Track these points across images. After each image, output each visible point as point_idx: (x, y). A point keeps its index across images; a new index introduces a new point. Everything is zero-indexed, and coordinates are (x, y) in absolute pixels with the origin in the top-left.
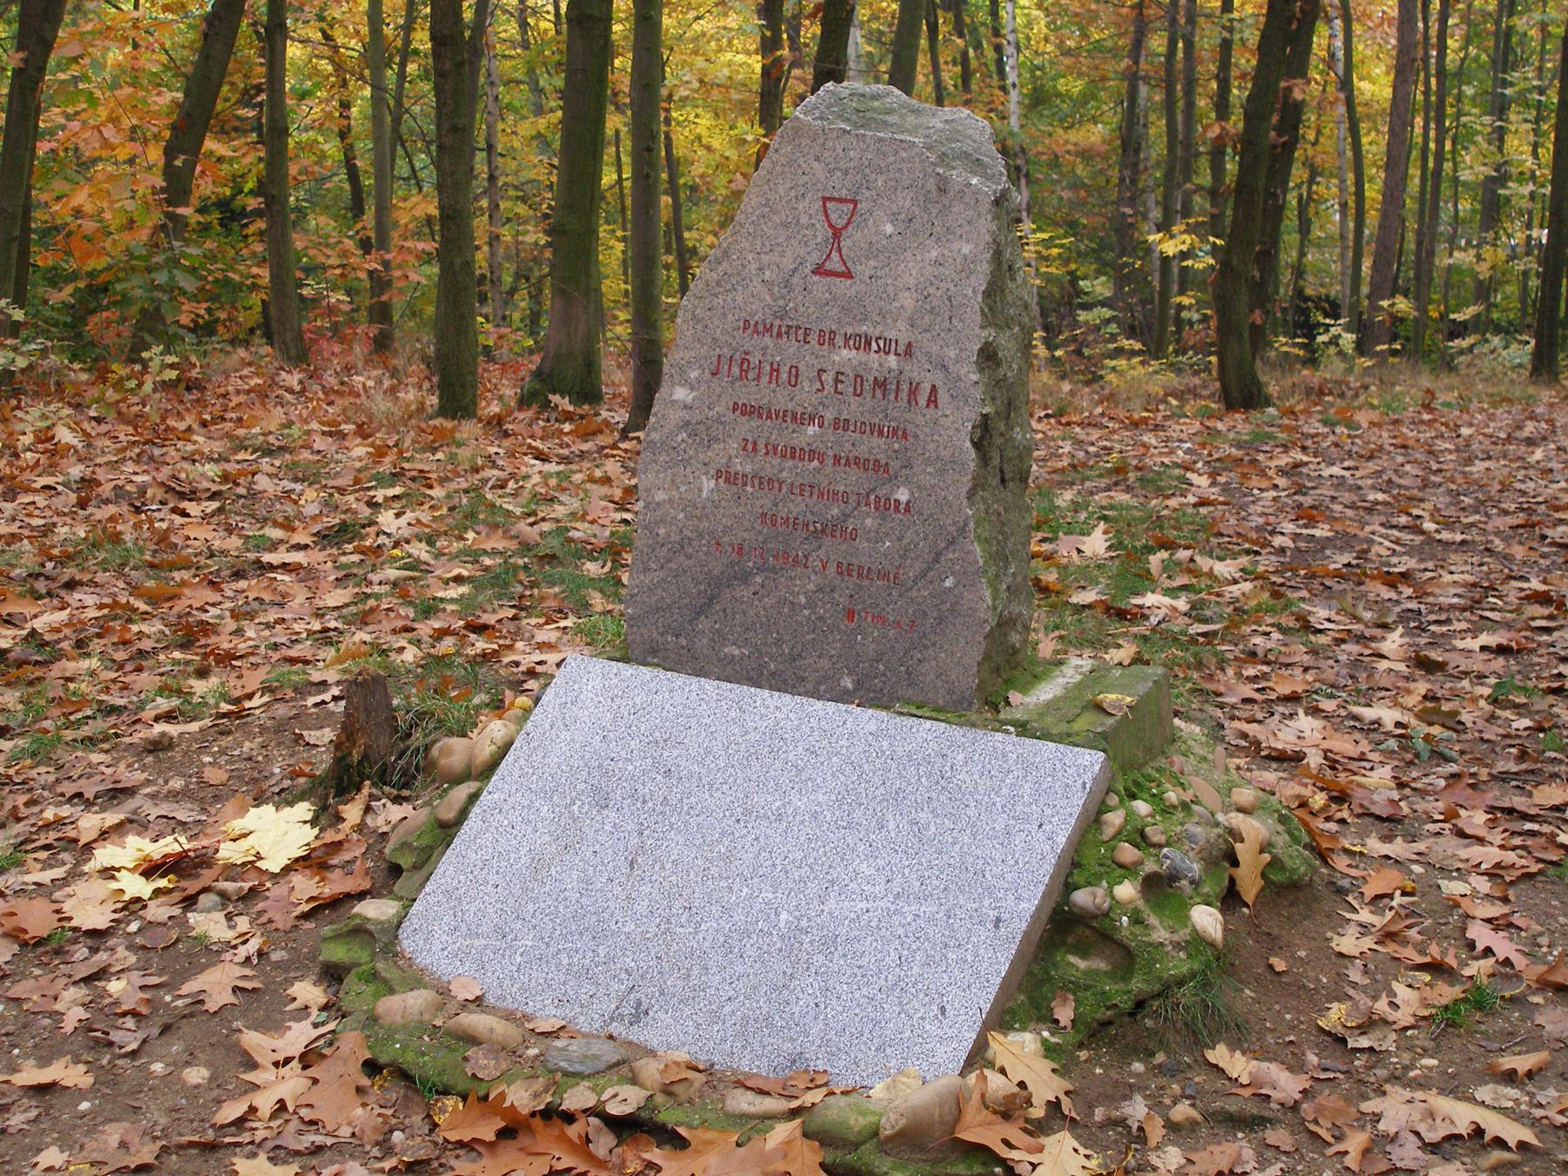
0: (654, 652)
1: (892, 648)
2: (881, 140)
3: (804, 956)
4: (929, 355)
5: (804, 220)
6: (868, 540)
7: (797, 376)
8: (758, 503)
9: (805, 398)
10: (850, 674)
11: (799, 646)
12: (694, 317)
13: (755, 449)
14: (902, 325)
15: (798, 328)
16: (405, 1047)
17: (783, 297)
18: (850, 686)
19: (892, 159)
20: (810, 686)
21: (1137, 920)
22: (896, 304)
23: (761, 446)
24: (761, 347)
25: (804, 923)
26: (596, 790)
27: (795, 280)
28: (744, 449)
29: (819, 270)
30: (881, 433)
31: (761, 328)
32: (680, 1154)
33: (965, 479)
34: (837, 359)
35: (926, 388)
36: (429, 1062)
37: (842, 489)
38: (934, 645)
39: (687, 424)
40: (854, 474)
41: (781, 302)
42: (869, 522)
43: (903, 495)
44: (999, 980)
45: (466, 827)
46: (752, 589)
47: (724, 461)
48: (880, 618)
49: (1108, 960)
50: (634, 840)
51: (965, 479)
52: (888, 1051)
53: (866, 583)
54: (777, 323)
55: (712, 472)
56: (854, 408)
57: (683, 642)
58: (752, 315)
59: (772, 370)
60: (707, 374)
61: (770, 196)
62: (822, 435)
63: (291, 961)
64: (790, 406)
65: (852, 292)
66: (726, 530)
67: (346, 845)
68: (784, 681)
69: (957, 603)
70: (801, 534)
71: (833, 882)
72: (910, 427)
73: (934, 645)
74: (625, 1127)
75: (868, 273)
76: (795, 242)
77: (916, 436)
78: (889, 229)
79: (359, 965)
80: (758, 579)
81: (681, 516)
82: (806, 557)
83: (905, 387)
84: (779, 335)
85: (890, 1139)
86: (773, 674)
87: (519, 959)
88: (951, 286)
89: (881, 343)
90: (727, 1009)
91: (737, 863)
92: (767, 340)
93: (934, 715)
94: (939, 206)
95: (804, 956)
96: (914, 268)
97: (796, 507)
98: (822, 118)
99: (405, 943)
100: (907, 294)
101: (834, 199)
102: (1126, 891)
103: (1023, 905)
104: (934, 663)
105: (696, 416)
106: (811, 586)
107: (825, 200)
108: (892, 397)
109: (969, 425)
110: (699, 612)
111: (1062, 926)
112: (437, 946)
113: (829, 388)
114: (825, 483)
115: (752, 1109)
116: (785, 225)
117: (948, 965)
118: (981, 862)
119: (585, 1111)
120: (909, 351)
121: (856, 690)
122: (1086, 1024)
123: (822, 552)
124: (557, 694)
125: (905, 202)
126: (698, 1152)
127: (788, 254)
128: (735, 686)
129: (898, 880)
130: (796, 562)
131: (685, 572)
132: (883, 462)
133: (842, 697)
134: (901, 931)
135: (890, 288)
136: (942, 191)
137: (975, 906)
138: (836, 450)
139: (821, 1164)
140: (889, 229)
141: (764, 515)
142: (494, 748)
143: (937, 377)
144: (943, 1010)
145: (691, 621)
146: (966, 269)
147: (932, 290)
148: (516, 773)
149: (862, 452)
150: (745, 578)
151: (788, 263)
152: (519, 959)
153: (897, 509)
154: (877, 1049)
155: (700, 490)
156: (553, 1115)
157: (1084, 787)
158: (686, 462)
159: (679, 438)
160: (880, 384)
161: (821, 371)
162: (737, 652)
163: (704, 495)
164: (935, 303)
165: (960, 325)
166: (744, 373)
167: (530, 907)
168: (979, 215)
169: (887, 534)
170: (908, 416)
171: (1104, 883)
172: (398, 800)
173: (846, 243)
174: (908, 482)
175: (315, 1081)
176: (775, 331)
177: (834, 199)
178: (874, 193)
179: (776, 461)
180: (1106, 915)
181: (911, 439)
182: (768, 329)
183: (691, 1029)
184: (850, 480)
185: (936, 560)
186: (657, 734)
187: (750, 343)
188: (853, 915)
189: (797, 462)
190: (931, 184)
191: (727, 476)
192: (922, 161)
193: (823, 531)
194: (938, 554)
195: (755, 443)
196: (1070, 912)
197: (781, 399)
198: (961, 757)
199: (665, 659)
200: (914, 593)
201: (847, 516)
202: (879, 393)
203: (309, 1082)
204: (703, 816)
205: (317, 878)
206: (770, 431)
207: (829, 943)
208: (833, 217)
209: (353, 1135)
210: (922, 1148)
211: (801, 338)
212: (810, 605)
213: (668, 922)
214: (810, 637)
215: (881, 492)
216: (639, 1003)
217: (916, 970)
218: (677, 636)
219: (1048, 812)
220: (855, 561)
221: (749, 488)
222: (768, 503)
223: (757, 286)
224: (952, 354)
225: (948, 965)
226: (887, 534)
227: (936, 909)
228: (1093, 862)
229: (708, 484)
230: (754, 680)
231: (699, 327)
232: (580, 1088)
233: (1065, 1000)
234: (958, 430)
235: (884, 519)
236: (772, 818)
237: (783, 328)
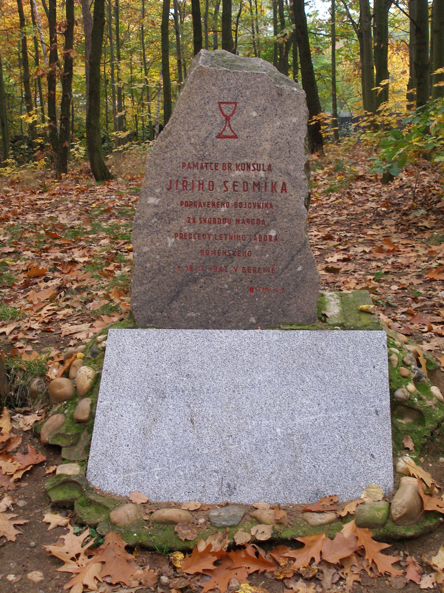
0: (150, 321)
1: (274, 302)
2: (246, 74)
3: (297, 446)
4: (280, 169)
5: (210, 113)
6: (257, 255)
7: (213, 186)
8: (198, 246)
9: (219, 194)
10: (253, 316)
11: (227, 308)
12: (155, 164)
13: (194, 221)
14: (266, 157)
15: (212, 163)
16: (139, 535)
17: (202, 150)
18: (254, 321)
19: (253, 82)
20: (234, 325)
21: (420, 399)
22: (261, 148)
23: (197, 220)
24: (191, 175)
25: (289, 431)
26: (156, 391)
27: (208, 142)
28: (189, 222)
29: (220, 136)
30: (259, 207)
31: (192, 166)
32: (301, 550)
33: (303, 222)
34: (233, 175)
35: (280, 184)
36: (157, 539)
37: (241, 234)
38: (295, 297)
39: (156, 214)
40: (247, 227)
41: (201, 153)
42: (257, 247)
43: (273, 233)
44: (390, 437)
45: (97, 421)
46: (199, 285)
47: (178, 229)
48: (267, 289)
49: (411, 417)
50: (188, 410)
51: (303, 222)
52: (357, 479)
53: (258, 274)
54: (200, 162)
55: (172, 235)
56: (244, 197)
57: (165, 314)
58: (187, 159)
59: (200, 184)
60: (165, 190)
61: (191, 104)
62: (228, 211)
63: (30, 505)
64: (211, 200)
65: (238, 144)
66: (183, 260)
67: (12, 441)
68: (220, 324)
69: (304, 277)
70: (222, 257)
71: (293, 410)
72: (273, 202)
73: (295, 297)
74: (272, 544)
75: (245, 135)
76: (206, 124)
77: (277, 206)
78: (254, 114)
79: (77, 499)
80: (202, 280)
81: (158, 257)
82: (226, 267)
83: (269, 185)
84: (202, 168)
85: (399, 518)
86: (214, 322)
87: (157, 478)
88: (289, 137)
89: (256, 167)
90: (273, 478)
91: (244, 410)
92: (196, 171)
93: (299, 327)
94: (280, 102)
95: (297, 446)
96: (269, 131)
97: (219, 245)
98: (213, 66)
99: (93, 483)
100: (267, 143)
101: (225, 103)
102: (411, 387)
103: (384, 403)
104: (295, 305)
105: (161, 210)
106: (230, 280)
107: (220, 103)
108: (263, 190)
109: (303, 199)
110: (172, 300)
111: (399, 407)
112: (111, 481)
113: (230, 189)
114: (233, 232)
115: (323, 521)
116: (201, 117)
117: (365, 436)
118: (356, 388)
119: (248, 543)
120: (270, 168)
121: (257, 322)
122: (419, 446)
123: (234, 264)
124: (112, 349)
125: (262, 101)
126: (310, 547)
127: (203, 129)
128: (201, 330)
129: (323, 404)
130: (221, 270)
131: (163, 282)
132: (261, 219)
133: (252, 327)
134: (336, 425)
135: (258, 141)
136: (280, 95)
137: (363, 407)
138: (237, 216)
139: (373, 538)
140: (254, 114)
141: (202, 251)
142: (90, 380)
143: (286, 179)
144: (372, 456)
145: (168, 304)
146: (295, 129)
147: (279, 140)
148: (111, 390)
149: (250, 216)
150: (195, 281)
151: (203, 134)
152: (157, 478)
153: (270, 240)
154: (352, 480)
155: (167, 244)
156: (234, 548)
157: (385, 347)
158: (158, 232)
159: (153, 221)
160: (257, 185)
161: (225, 182)
162: (194, 315)
163: (170, 245)
164: (281, 145)
165: (294, 155)
166: (185, 187)
167: (150, 452)
168: (300, 104)
169: (267, 251)
170: (272, 198)
171: (404, 386)
172: (26, 413)
173: (232, 123)
174: (275, 227)
175: (103, 563)
176: (199, 166)
177: (225, 103)
178: (245, 98)
179: (206, 226)
180: (409, 399)
181: (275, 208)
182: (196, 166)
183: (261, 491)
184: (246, 229)
185: (292, 260)
186: (173, 359)
187: (186, 173)
188: (310, 423)
189: (217, 224)
190: (274, 92)
191: (182, 236)
192: (268, 82)
193: (234, 254)
194: (293, 257)
195: (194, 219)
196: (397, 401)
197: (206, 197)
198: (323, 344)
199: (156, 323)
200: (283, 276)
201: (245, 246)
202: (256, 189)
203: (100, 565)
204: (216, 393)
205: (10, 460)
206: (201, 212)
207: (305, 438)
208: (225, 111)
209: (140, 584)
210: (413, 519)
211: (213, 168)
212: (231, 288)
213: (224, 444)
214: (231, 302)
215: (262, 233)
216: (229, 486)
217: (351, 441)
218: (161, 312)
219: (374, 361)
220: (252, 266)
221: (193, 240)
222: (204, 245)
223: (187, 146)
224: (292, 167)
225: (365, 436)
226: (267, 251)
227: (346, 412)
228: (395, 378)
229: (171, 241)
230: (205, 326)
231: (158, 168)
232: (239, 532)
233: (407, 439)
234: (298, 201)
235: (264, 245)
236: (250, 387)
237: (204, 164)
